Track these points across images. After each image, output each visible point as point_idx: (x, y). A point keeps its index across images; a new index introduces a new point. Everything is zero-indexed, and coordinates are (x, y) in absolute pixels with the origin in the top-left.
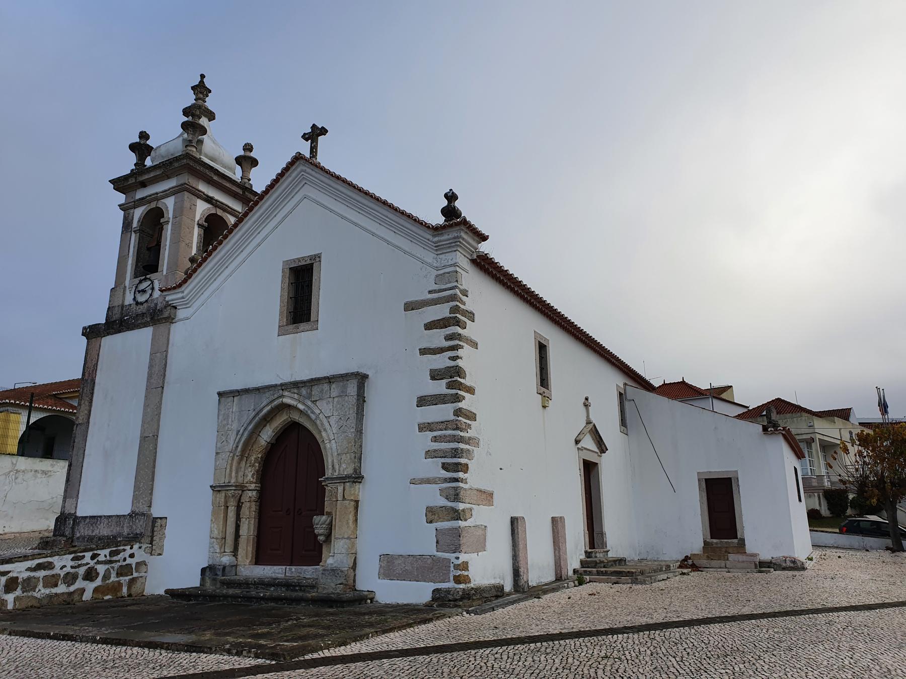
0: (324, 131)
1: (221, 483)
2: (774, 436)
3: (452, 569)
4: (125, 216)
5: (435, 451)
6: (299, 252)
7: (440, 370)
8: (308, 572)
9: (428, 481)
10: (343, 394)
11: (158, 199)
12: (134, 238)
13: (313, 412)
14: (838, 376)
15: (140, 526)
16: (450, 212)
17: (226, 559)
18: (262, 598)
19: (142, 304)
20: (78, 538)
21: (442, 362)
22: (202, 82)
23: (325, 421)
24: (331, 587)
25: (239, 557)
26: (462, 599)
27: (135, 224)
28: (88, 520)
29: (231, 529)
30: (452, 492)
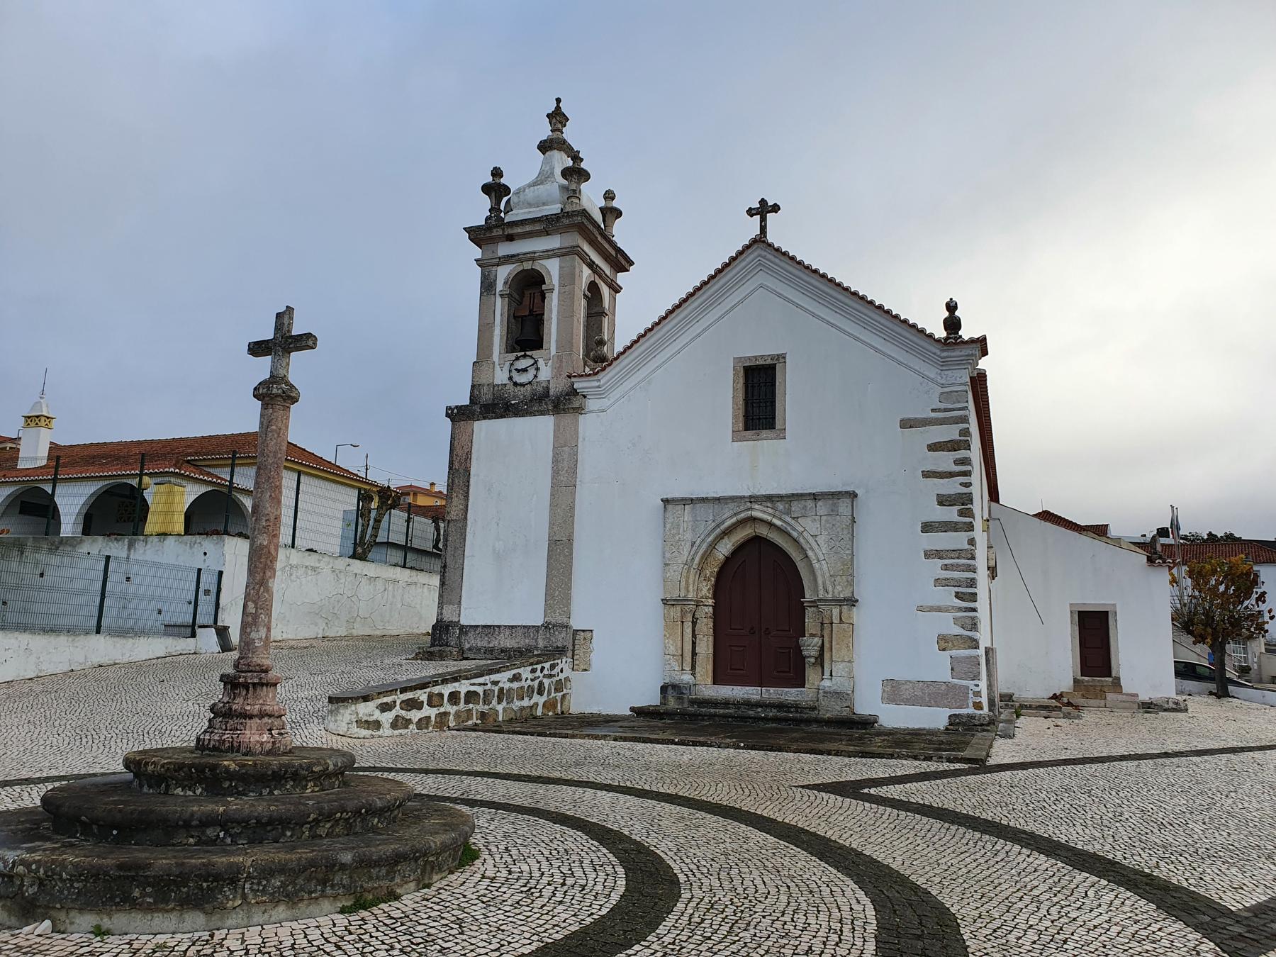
0: (776, 208)
1: (675, 596)
2: (1160, 569)
3: (971, 695)
4: (482, 273)
5: (946, 579)
6: (759, 349)
7: (950, 496)
8: (790, 694)
9: (939, 609)
10: (833, 512)
11: (533, 259)
12: (500, 306)
13: (795, 530)
14: (1211, 497)
15: (560, 639)
16: (952, 324)
17: (687, 678)
18: (763, 719)
19: (522, 385)
20: (470, 649)
21: (952, 487)
22: (558, 108)
23: (811, 540)
24: (832, 709)
25: (698, 675)
26: (988, 725)
27: (500, 286)
28: (480, 630)
29: (688, 647)
30: (969, 621)
